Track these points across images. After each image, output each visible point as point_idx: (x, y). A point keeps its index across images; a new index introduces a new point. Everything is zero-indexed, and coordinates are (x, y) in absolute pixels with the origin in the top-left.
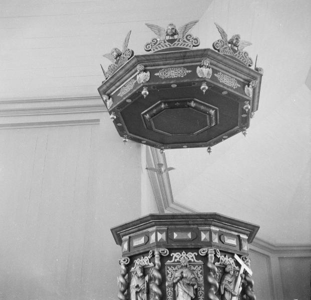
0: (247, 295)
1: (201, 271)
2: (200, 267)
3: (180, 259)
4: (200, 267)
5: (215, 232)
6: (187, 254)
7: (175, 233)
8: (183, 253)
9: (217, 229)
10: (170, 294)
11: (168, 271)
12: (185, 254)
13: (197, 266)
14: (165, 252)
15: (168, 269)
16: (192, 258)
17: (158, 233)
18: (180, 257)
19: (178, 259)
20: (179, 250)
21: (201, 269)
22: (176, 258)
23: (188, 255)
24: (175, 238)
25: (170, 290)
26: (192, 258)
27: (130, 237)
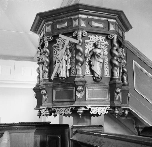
0: (95, 77)
1: (107, 49)
2: (107, 46)
3: (94, 40)
4: (107, 46)
5: (84, 19)
6: (98, 37)
7: (57, 25)
8: (96, 36)
9: (86, 17)
10: (106, 63)
11: (86, 47)
12: (98, 37)
13: (104, 46)
14: (51, 38)
15: (86, 46)
16: (102, 40)
17: (46, 27)
18: (61, 40)
19: (93, 40)
20: (95, 33)
21: (107, 48)
22: (92, 39)
23: (99, 38)
24: (57, 28)
25: (106, 61)
26: (102, 40)
27: (72, 29)
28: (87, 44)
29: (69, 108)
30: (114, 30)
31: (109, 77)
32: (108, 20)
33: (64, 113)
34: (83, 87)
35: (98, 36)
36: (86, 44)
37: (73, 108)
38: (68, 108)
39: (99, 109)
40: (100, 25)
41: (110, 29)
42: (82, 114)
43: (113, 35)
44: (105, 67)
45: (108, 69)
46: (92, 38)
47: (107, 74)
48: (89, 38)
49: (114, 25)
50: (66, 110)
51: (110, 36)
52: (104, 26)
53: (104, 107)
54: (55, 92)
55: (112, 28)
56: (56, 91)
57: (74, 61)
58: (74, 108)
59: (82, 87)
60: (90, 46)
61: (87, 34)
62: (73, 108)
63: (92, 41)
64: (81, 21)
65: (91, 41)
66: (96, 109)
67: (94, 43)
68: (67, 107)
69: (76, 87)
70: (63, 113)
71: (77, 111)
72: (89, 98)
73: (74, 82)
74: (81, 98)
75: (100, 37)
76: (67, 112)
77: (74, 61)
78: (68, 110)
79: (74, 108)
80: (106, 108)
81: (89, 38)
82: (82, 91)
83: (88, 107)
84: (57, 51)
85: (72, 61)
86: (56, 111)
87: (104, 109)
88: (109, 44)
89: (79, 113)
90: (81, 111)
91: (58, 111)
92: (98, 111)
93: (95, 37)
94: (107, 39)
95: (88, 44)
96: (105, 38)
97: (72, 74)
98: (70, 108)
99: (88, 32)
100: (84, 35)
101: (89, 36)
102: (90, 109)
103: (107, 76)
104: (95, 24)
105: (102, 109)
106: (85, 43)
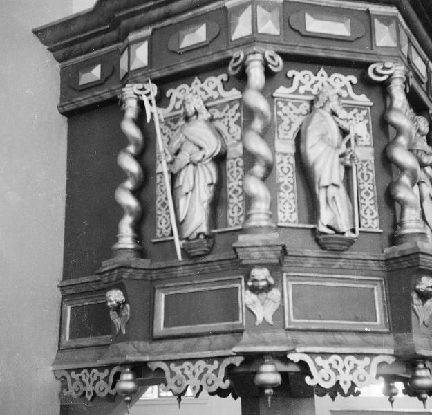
4: (364, 112)
6: (329, 76)
19: (307, 87)
22: (301, 84)
28: (286, 103)
29: (109, 373)
30: (277, 33)
31: (381, 231)
32: (368, 11)
33: (94, 392)
34: (276, 268)
35: (326, 75)
36: (281, 104)
37: (238, 364)
38: (216, 363)
39: (347, 366)
40: (340, 29)
41: (378, 45)
42: (275, 387)
43: (388, 65)
44: (291, 187)
45: (292, 195)
46: (303, 81)
47: (372, 221)
48: (289, 82)
49: (393, 25)
50: (206, 369)
51: (374, 69)
52: (352, 32)
53: (367, 359)
54: (161, 298)
55: (384, 37)
56: (167, 294)
57: (370, 173)
58: (238, 361)
59: (179, 275)
60: (297, 111)
61: (284, 64)
62: (238, 364)
63: (302, 90)
64: (378, 24)
65: (296, 92)
66: (330, 365)
67: (311, 98)
68: (209, 360)
69: (246, 271)
70: (89, 393)
71: (255, 373)
72: (298, 321)
73: (234, 249)
74: (271, 322)
75: (334, 76)
76: (327, 378)
77: (238, 171)
78: (216, 372)
79: (238, 361)
80: (377, 360)
81: (289, 82)
82: (268, 287)
83: (295, 357)
84: (169, 137)
85: (232, 172)
86: (168, 374)
87: (367, 364)
88: (371, 104)
89: (263, 387)
90: (269, 374)
91: (72, 383)
92: (191, 376)
93: (314, 79)
94: (366, 84)
95: (290, 104)
96: (355, 80)
97: (230, 221)
98: (227, 362)
99: (285, 57)
100: (275, 66)
101: (290, 74)
102: (302, 364)
103: (288, 221)
104: (314, 25)
105: (98, 377)
106: (276, 99)
